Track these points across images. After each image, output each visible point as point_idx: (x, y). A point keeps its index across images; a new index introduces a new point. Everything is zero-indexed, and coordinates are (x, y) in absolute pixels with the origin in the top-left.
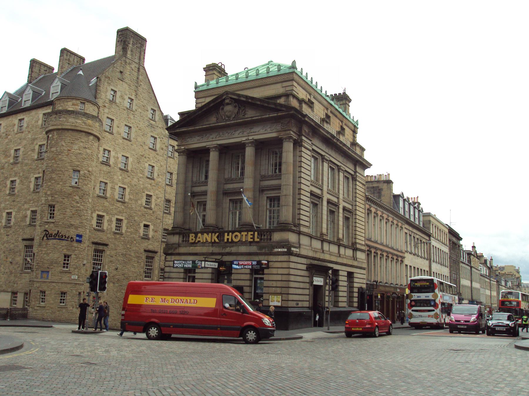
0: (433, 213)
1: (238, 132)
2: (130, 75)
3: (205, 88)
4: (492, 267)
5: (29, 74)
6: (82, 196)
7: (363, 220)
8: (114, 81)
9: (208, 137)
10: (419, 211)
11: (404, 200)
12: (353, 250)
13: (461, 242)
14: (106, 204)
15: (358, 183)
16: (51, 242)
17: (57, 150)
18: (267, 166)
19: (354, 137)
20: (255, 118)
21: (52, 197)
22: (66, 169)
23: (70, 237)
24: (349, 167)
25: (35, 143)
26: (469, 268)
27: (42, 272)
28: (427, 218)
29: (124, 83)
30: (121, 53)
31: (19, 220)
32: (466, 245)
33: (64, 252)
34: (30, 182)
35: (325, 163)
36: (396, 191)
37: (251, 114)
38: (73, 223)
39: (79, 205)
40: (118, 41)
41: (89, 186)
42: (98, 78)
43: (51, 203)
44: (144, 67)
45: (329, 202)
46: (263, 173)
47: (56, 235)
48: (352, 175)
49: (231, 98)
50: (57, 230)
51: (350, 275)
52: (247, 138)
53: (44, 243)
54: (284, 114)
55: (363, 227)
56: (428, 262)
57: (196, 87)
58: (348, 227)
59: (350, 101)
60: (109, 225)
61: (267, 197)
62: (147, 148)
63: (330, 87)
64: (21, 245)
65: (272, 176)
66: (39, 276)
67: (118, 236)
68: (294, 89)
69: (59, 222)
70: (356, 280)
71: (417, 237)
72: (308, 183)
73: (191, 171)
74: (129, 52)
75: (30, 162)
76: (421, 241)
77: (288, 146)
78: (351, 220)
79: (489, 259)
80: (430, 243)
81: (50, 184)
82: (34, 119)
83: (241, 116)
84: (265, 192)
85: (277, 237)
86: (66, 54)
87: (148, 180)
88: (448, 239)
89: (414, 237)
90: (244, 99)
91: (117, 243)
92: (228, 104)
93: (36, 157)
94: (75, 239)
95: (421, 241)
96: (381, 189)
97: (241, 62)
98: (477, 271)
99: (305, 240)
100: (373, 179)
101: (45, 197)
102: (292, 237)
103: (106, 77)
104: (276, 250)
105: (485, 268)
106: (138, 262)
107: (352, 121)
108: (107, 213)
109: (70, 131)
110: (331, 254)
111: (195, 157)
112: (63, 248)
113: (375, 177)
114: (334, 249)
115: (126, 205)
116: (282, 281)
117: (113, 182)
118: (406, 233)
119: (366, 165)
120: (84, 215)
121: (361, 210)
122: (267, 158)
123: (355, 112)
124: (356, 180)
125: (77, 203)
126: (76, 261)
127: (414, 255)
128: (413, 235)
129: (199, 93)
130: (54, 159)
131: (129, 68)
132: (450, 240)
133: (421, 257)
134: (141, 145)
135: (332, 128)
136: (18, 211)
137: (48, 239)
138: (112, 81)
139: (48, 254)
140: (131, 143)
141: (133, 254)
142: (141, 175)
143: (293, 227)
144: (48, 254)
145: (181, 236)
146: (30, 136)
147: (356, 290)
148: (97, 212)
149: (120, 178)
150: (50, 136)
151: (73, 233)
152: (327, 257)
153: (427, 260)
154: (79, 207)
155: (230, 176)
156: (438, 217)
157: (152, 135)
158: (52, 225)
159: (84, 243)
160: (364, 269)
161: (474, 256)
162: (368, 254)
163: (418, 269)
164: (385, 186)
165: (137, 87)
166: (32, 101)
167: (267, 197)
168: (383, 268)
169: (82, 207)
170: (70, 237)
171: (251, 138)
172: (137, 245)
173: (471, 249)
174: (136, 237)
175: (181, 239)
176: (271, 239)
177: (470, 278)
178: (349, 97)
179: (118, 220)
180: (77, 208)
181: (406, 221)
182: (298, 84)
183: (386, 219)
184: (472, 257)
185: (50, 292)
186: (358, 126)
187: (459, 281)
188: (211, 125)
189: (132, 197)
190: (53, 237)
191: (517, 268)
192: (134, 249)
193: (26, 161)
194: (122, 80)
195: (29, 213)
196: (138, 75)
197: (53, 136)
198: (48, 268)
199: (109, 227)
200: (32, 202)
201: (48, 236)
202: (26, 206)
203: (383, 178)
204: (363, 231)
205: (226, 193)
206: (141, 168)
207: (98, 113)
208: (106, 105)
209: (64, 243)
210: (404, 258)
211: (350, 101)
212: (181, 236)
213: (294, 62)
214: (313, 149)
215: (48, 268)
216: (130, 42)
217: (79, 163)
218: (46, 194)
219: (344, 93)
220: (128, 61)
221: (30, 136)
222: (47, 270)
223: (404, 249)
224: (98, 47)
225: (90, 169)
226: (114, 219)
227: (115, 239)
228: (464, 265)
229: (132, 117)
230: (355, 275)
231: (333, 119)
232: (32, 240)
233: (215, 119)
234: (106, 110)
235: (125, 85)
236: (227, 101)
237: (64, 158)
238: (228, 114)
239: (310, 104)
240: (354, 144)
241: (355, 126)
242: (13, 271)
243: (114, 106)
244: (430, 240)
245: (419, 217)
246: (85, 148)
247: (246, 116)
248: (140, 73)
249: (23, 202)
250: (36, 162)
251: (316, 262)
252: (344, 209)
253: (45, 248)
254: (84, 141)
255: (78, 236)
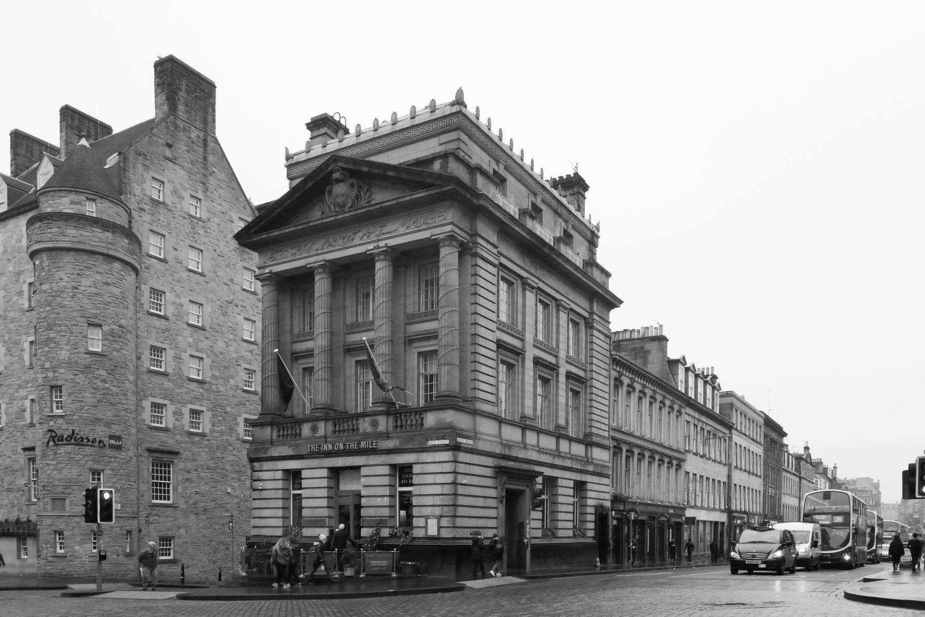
0: (739, 393)
1: (360, 235)
2: (188, 151)
3: (303, 157)
4: (835, 479)
5: (12, 160)
6: (113, 370)
7: (606, 396)
8: (156, 162)
9: (310, 248)
10: (714, 388)
11: (687, 369)
12: (587, 445)
13: (786, 440)
14: (168, 384)
15: (595, 333)
16: (62, 450)
17: (51, 288)
18: (417, 297)
19: (592, 253)
20: (387, 204)
21: (54, 372)
22: (73, 322)
23: (98, 440)
24: (580, 303)
25: (21, 280)
26: (797, 479)
27: (54, 499)
28: (727, 400)
29: (177, 167)
30: (166, 108)
31: (14, 416)
32: (794, 444)
33: (87, 466)
34: (23, 350)
35: (561, 313)
36: (673, 353)
37: (381, 197)
38: (99, 416)
39: (107, 385)
40: (157, 85)
41: (125, 352)
42: (120, 154)
43: (54, 383)
44: (216, 139)
45: (537, 362)
46: (410, 310)
47: (70, 437)
48: (584, 318)
49: (343, 169)
50: (71, 428)
51: (580, 487)
52: (375, 244)
53: (50, 453)
54: (433, 192)
55: (606, 409)
56: (726, 468)
57: (288, 158)
58: (577, 408)
59: (586, 188)
60: (177, 419)
61: (419, 353)
62: (237, 288)
63: (549, 166)
64: (22, 458)
65: (426, 314)
66: (49, 507)
67: (196, 439)
68: (462, 146)
69: (73, 415)
70: (590, 494)
71: (708, 428)
72: (493, 326)
73: (288, 315)
74: (181, 107)
75: (17, 315)
76: (714, 435)
77: (449, 256)
78: (582, 395)
79: (831, 467)
80: (731, 438)
81: (47, 349)
82: (14, 236)
83: (363, 203)
84: (415, 345)
85: (430, 419)
86: (71, 118)
87: (245, 344)
88: (763, 434)
89: (702, 429)
90: (365, 169)
91: (196, 450)
92: (338, 181)
93: (26, 306)
94: (107, 444)
95: (714, 435)
96: (648, 352)
97: (372, 105)
98: (809, 484)
99: (487, 427)
100: (635, 336)
101: (42, 372)
102: (461, 420)
103: (139, 154)
104: (431, 443)
105: (823, 480)
106: (239, 480)
107: (588, 224)
108: (171, 400)
109: (71, 253)
110: (541, 451)
111: (291, 287)
112: (86, 459)
113: (639, 331)
114: (548, 442)
115: (206, 386)
116: (442, 495)
117: (176, 347)
118: (688, 422)
119: (611, 302)
120: (120, 403)
121: (602, 379)
122: (417, 282)
123: (594, 209)
124: (592, 328)
125: (104, 381)
126: (114, 480)
127: (703, 456)
128: (700, 425)
129: (292, 164)
130: (50, 304)
131: (184, 138)
132: (765, 435)
133: (715, 461)
134: (226, 284)
135: (546, 231)
136: (10, 402)
137: (56, 445)
138: (152, 163)
139: (60, 471)
140: (206, 279)
141: (228, 467)
142: (231, 336)
143: (461, 401)
144: (60, 471)
145: (275, 428)
146: (11, 268)
147: (591, 510)
148: (152, 399)
149: (191, 340)
150: (37, 262)
151: (101, 432)
152: (534, 456)
153: (725, 465)
154: (108, 389)
155: (354, 320)
156: (748, 400)
157: (246, 265)
158: (60, 421)
159: (128, 450)
160: (607, 476)
161: (806, 462)
162: (615, 454)
163: (714, 480)
164: (653, 347)
165: (204, 176)
166: (9, 205)
167: (419, 353)
168: (644, 475)
169: (114, 389)
170: (98, 440)
171: (382, 244)
172: (235, 452)
173: (802, 452)
174: (232, 439)
175: (275, 433)
176: (422, 425)
177: (798, 495)
178: (584, 181)
179: (193, 412)
180: (105, 391)
181: (686, 401)
182: (470, 138)
183: (651, 397)
184: (802, 463)
185: (70, 533)
186: (600, 234)
187: (780, 499)
188: (311, 224)
189: (217, 374)
190: (65, 442)
191: (875, 481)
192: (230, 458)
193: (11, 314)
194: (172, 160)
195: (27, 403)
196: (205, 152)
197: (41, 262)
198: (63, 493)
199: (178, 423)
200: (30, 385)
201: (56, 439)
202: (22, 393)
203: (652, 333)
204: (606, 415)
205: (350, 350)
206: (230, 324)
207: (130, 222)
208: (146, 207)
209: (88, 450)
210: (684, 460)
211: (586, 188)
212: (275, 428)
213: (460, 93)
214: (501, 264)
215: (63, 493)
216: (183, 88)
217: (98, 311)
218: (43, 367)
219: (576, 174)
220: (180, 123)
221: (11, 268)
222: (62, 496)
223: (681, 447)
224: (128, 105)
225: (123, 322)
226: (186, 411)
227: (192, 443)
228: (788, 475)
229: (201, 231)
230: (589, 486)
231: (547, 214)
232: (33, 449)
233: (320, 213)
234: (147, 217)
235: (181, 172)
236: (336, 175)
237: (67, 303)
238: (340, 200)
239: (499, 181)
240: (591, 262)
241: (593, 233)
242: (16, 502)
243: (161, 210)
244: (731, 433)
245: (713, 399)
246: (107, 284)
247: (373, 203)
248: (209, 149)
249: (15, 386)
250: (28, 314)
251: (511, 464)
252: (569, 375)
253: (52, 460)
254: (101, 270)
255: (111, 437)
